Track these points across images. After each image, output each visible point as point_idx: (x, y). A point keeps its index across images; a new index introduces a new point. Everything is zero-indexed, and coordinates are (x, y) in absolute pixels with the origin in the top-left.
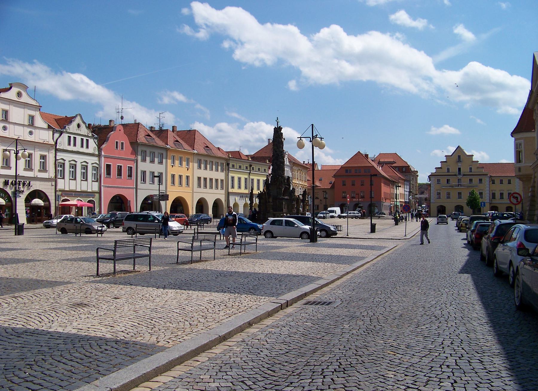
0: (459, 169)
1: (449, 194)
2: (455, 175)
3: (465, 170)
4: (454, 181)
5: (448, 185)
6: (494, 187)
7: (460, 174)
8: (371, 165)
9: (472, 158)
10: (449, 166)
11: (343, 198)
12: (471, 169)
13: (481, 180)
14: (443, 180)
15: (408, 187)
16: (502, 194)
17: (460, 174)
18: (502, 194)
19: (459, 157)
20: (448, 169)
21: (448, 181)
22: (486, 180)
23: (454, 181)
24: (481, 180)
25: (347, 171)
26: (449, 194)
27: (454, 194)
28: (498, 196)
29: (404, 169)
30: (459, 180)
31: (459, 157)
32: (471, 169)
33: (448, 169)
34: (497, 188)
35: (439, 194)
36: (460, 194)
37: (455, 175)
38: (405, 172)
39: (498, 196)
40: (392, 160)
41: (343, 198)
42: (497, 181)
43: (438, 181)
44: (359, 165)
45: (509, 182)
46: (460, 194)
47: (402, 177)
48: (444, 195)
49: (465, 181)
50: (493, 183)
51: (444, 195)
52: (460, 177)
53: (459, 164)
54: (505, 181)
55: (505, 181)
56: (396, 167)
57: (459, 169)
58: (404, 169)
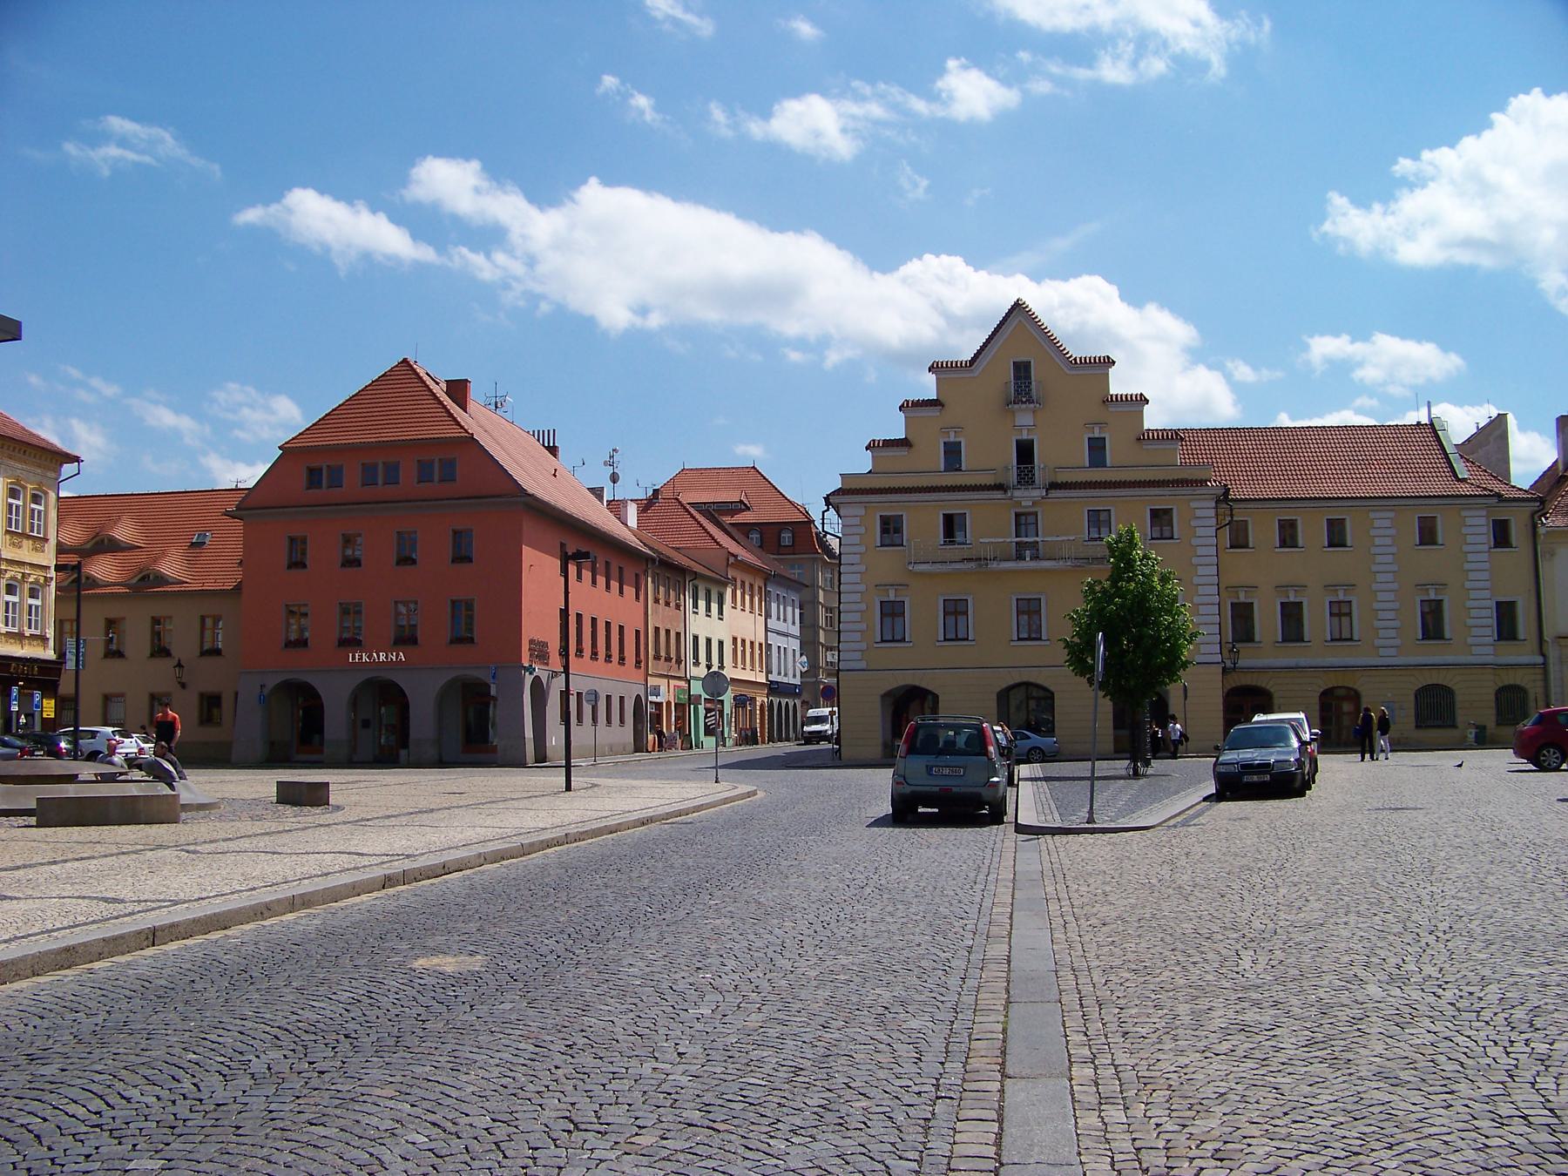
0: (1025, 452)
1: (955, 609)
2: (999, 487)
3: (1060, 452)
4: (988, 526)
5: (953, 551)
6: (1243, 567)
7: (1026, 477)
8: (454, 432)
9: (1105, 379)
10: (958, 429)
11: (289, 644)
12: (1097, 447)
13: (1160, 517)
14: (922, 523)
15: (793, 613)
16: (1292, 615)
17: (1026, 477)
18: (1292, 615)
19: (1022, 370)
20: (953, 453)
21: (951, 525)
22: (1198, 521)
23: (988, 526)
24: (1160, 517)
25: (314, 476)
26: (955, 609)
27: (992, 611)
28: (1267, 622)
29: (786, 537)
30: (1023, 521)
31: (1022, 370)
32: (1097, 447)
33: (953, 453)
34: (1266, 573)
35: (892, 611)
36: (1029, 609)
37: (999, 487)
38: (793, 549)
39: (1267, 622)
40: (733, 496)
41: (289, 644)
42: (1264, 532)
43: (891, 528)
44: (388, 436)
45: (1336, 534)
46: (1029, 609)
47: (743, 554)
48: (923, 617)
49: (1063, 524)
50: (1239, 541)
51: (923, 617)
52: (1027, 497)
53: (1024, 418)
54: (1312, 531)
55: (1312, 531)
56: (746, 529)
57: (1025, 452)
58: (786, 537)
